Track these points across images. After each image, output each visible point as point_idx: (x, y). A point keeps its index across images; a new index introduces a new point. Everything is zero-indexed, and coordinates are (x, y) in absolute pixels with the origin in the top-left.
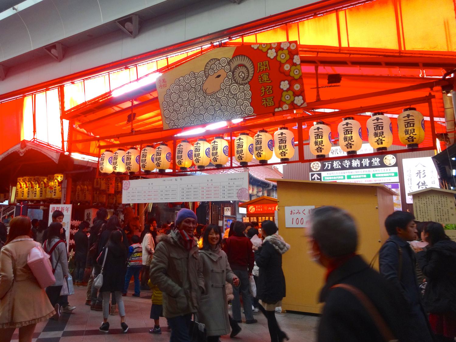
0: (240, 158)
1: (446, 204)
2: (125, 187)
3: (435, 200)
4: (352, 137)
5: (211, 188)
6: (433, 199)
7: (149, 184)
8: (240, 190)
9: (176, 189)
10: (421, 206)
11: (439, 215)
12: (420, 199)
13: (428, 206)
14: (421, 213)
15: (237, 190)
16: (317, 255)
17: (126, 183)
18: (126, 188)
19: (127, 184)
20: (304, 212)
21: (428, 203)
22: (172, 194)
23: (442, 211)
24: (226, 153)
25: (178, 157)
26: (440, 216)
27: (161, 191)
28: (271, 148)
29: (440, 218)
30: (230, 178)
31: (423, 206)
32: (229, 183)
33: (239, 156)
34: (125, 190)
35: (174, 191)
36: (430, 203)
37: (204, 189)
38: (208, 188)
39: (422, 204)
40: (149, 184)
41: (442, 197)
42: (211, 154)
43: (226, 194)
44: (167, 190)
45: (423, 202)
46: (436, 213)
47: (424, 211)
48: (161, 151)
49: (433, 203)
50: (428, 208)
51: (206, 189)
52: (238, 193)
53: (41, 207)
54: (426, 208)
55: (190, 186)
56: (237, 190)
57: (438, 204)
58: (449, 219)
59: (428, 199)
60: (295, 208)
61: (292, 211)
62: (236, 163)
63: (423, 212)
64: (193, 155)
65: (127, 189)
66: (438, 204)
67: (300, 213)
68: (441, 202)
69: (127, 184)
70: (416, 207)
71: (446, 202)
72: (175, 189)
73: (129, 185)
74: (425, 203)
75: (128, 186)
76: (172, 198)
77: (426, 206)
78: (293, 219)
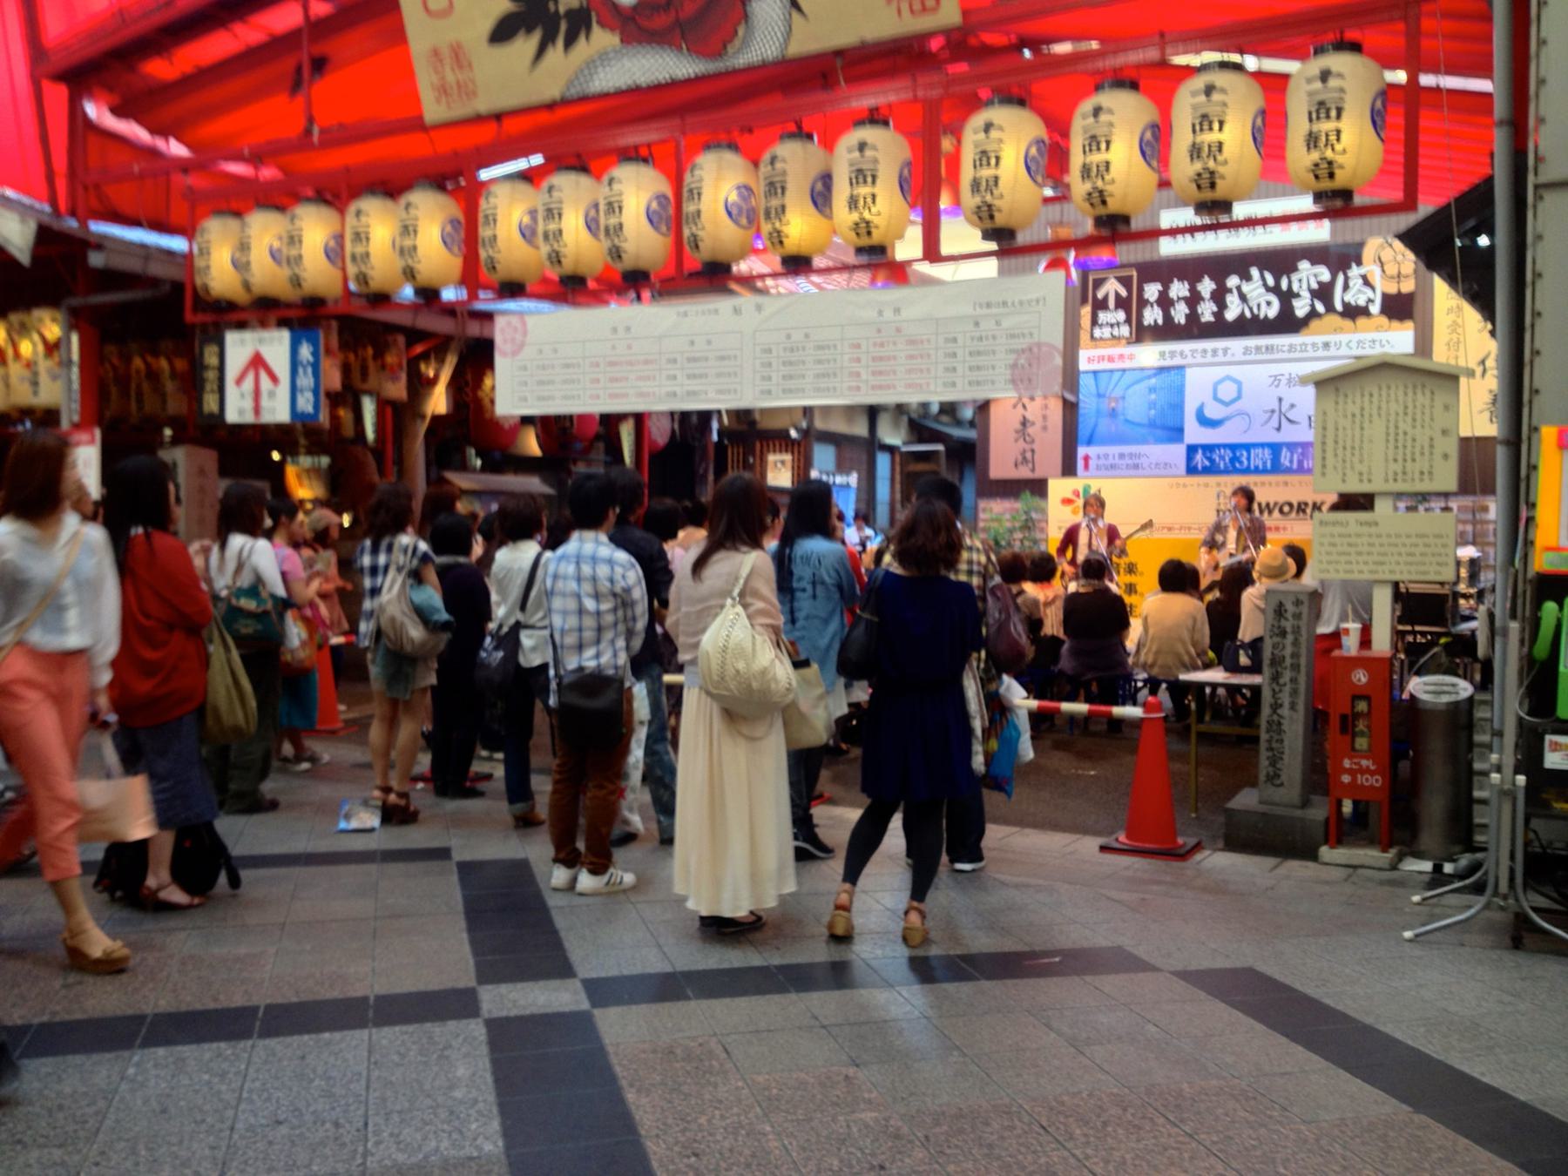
2: (505, 341)
7: (615, 330)
8: (1023, 351)
10: (1342, 422)
11: (1400, 458)
12: (1341, 400)
13: (1366, 425)
16: (844, 565)
19: (515, 329)
23: (1409, 444)
29: (1399, 470)
34: (504, 354)
35: (726, 363)
36: (1375, 412)
37: (775, 353)
38: (792, 350)
39: (1345, 416)
40: (615, 330)
41: (1419, 392)
45: (1351, 408)
49: (1383, 413)
52: (1014, 366)
53: (1140, 684)
55: (797, 336)
58: (1430, 473)
59: (1367, 398)
68: (1410, 411)
71: (1427, 411)
73: (525, 333)
74: (1358, 412)
75: (518, 337)
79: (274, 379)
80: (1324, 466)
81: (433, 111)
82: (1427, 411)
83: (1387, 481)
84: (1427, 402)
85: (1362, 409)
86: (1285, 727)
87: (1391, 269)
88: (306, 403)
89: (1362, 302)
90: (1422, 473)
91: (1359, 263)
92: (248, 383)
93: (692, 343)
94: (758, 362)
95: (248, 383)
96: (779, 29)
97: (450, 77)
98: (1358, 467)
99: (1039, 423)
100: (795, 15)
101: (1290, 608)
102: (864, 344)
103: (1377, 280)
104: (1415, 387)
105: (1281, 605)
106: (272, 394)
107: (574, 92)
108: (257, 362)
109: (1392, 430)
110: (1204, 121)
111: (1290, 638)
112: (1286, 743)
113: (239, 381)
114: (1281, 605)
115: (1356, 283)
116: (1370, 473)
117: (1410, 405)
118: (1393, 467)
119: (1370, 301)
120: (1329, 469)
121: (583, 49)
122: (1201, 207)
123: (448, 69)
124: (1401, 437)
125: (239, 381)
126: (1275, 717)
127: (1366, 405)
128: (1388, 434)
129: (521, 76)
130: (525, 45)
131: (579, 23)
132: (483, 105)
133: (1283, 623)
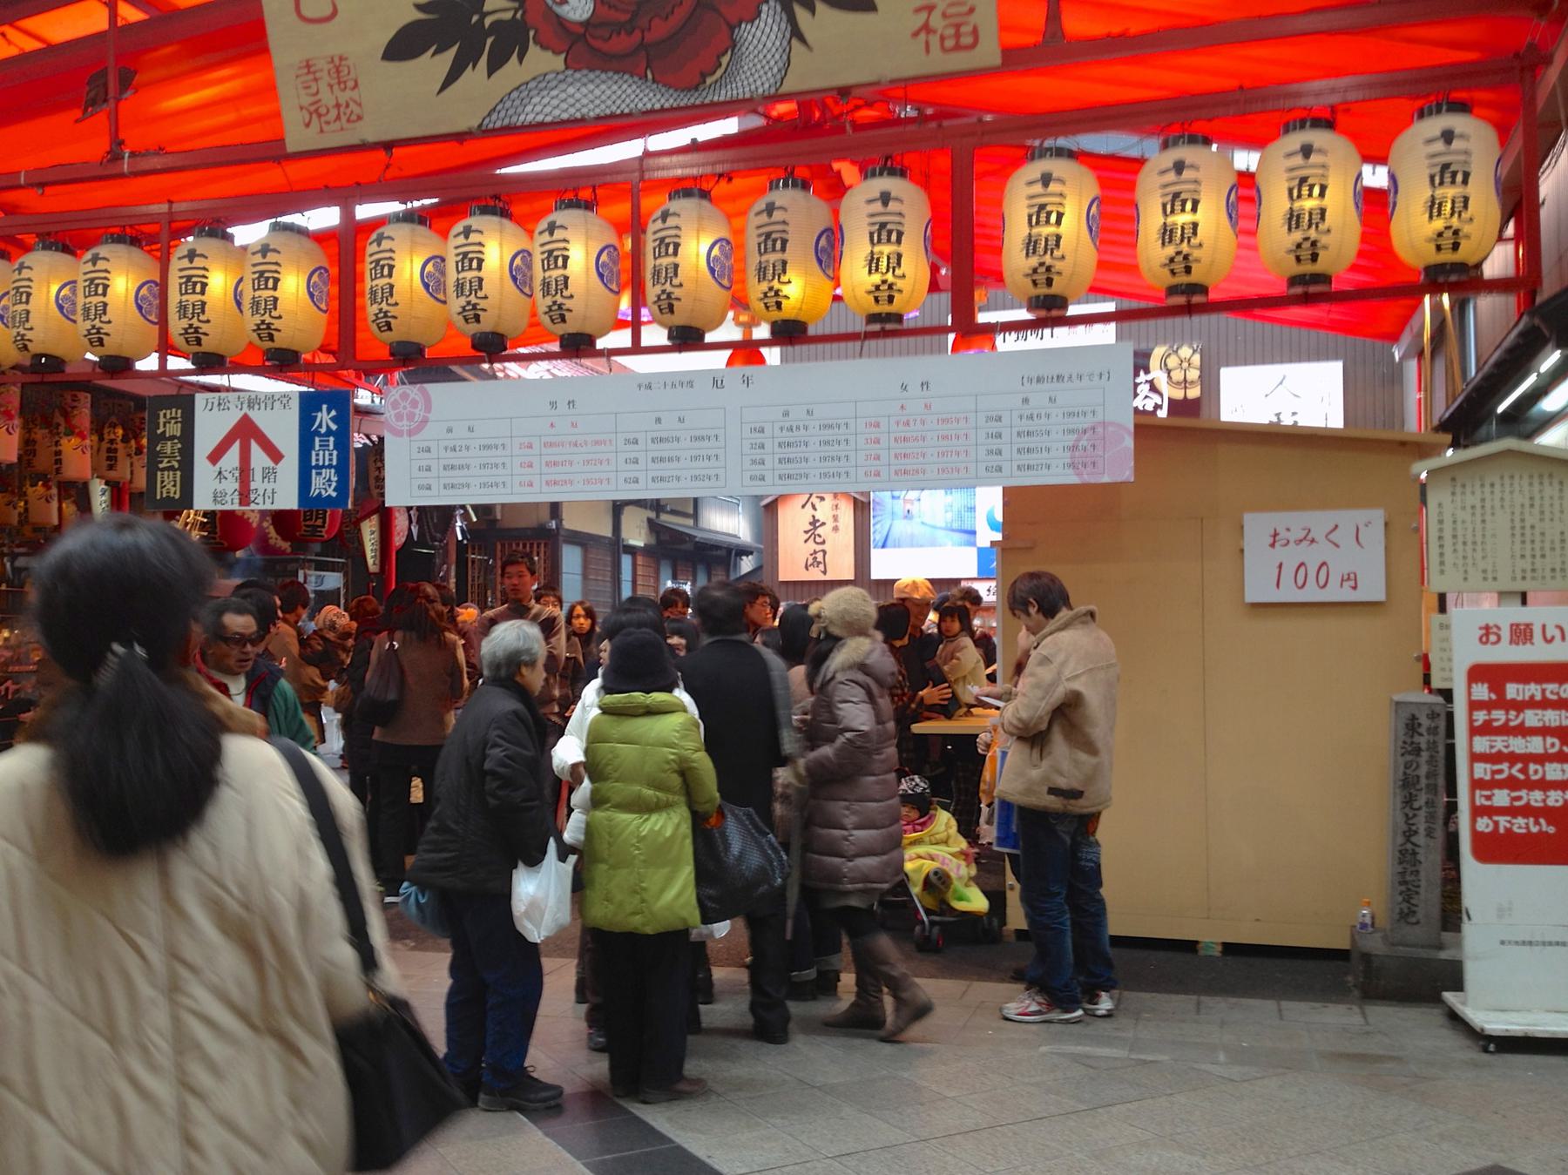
0: (668, 305)
1: (1557, 507)
3: (1516, 494)
4: (1195, 225)
5: (468, 448)
6: (1507, 489)
8: (1085, 432)
9: (721, 433)
10: (1461, 515)
11: (1528, 553)
12: (1458, 490)
13: (1488, 518)
14: (1460, 547)
15: (1071, 431)
17: (405, 396)
18: (404, 425)
19: (414, 404)
20: (1331, 537)
21: (1488, 505)
22: (484, 466)
23: (1538, 538)
24: (611, 281)
25: (656, 273)
26: (1529, 559)
27: (628, 441)
28: (437, 290)
29: (1529, 567)
30: (1034, 375)
31: (1468, 518)
32: (1026, 401)
33: (191, 326)
36: (1497, 503)
39: (1464, 508)
40: (553, 405)
41: (1546, 481)
42: (451, 288)
43: (768, 464)
44: (458, 443)
46: (1518, 546)
47: (1469, 539)
48: (677, 227)
49: (1507, 504)
50: (1488, 525)
51: (894, 427)
52: (1074, 448)
54: (1479, 526)
56: (1071, 431)
57: (1527, 509)
58: (1563, 570)
59: (1487, 489)
60: (1293, 522)
61: (1276, 535)
62: (654, 335)
63: (1465, 543)
64: (451, 288)
65: (410, 433)
66: (1527, 509)
67: (1313, 541)
68: (1537, 502)
69: (414, 404)
70: (1441, 522)
71: (1557, 503)
72: (499, 442)
73: (428, 408)
74: (1478, 505)
76: (484, 485)
77: (1478, 518)
78: (1280, 566)
79: (275, 455)
80: (1442, 563)
81: (298, 137)
82: (1557, 503)
83: (1514, 579)
84: (1556, 494)
85: (1483, 500)
86: (1421, 857)
87: (1177, 375)
88: (324, 484)
89: (1150, 408)
90: (1553, 570)
91: (1147, 371)
92: (232, 458)
93: (659, 420)
94: (747, 444)
95: (232, 458)
96: (775, 61)
97: (327, 98)
98: (1482, 565)
99: (830, 524)
100: (794, 42)
101: (1425, 722)
102: (884, 422)
103: (1163, 384)
104: (1541, 476)
105: (1414, 718)
106: (268, 474)
107: (497, 122)
108: (246, 432)
109: (1518, 524)
110: (1040, 213)
111: (1425, 755)
112: (1422, 874)
113: (215, 457)
114: (1414, 718)
115: (1144, 389)
116: (1494, 571)
117: (1537, 497)
118: (1521, 564)
119: (1157, 407)
120: (1448, 567)
121: (513, 72)
122: (1033, 304)
123: (323, 86)
124: (1528, 531)
125: (215, 457)
126: (1409, 846)
127: (1487, 495)
128: (1513, 528)
129: (420, 100)
130: (435, 64)
131: (508, 42)
132: (369, 132)
133: (1417, 739)
